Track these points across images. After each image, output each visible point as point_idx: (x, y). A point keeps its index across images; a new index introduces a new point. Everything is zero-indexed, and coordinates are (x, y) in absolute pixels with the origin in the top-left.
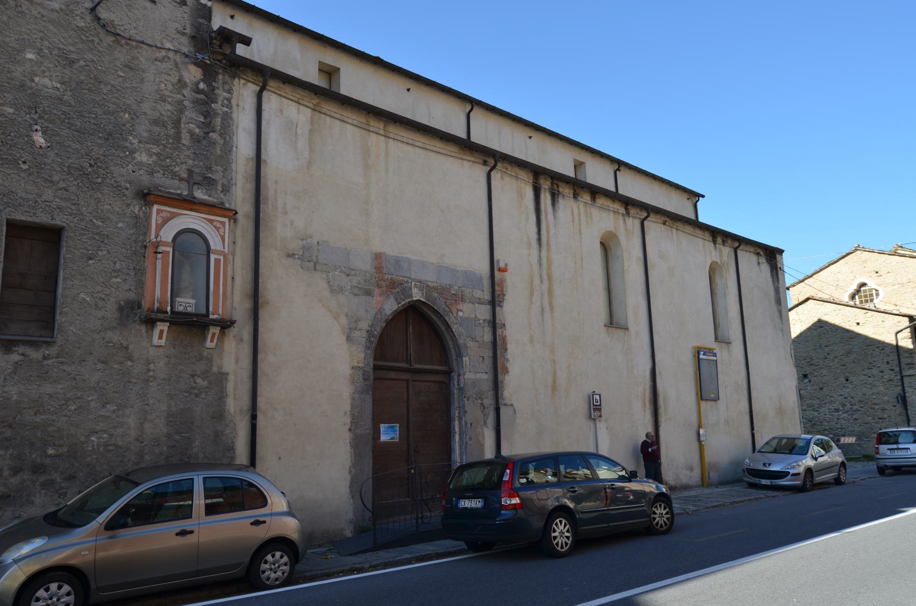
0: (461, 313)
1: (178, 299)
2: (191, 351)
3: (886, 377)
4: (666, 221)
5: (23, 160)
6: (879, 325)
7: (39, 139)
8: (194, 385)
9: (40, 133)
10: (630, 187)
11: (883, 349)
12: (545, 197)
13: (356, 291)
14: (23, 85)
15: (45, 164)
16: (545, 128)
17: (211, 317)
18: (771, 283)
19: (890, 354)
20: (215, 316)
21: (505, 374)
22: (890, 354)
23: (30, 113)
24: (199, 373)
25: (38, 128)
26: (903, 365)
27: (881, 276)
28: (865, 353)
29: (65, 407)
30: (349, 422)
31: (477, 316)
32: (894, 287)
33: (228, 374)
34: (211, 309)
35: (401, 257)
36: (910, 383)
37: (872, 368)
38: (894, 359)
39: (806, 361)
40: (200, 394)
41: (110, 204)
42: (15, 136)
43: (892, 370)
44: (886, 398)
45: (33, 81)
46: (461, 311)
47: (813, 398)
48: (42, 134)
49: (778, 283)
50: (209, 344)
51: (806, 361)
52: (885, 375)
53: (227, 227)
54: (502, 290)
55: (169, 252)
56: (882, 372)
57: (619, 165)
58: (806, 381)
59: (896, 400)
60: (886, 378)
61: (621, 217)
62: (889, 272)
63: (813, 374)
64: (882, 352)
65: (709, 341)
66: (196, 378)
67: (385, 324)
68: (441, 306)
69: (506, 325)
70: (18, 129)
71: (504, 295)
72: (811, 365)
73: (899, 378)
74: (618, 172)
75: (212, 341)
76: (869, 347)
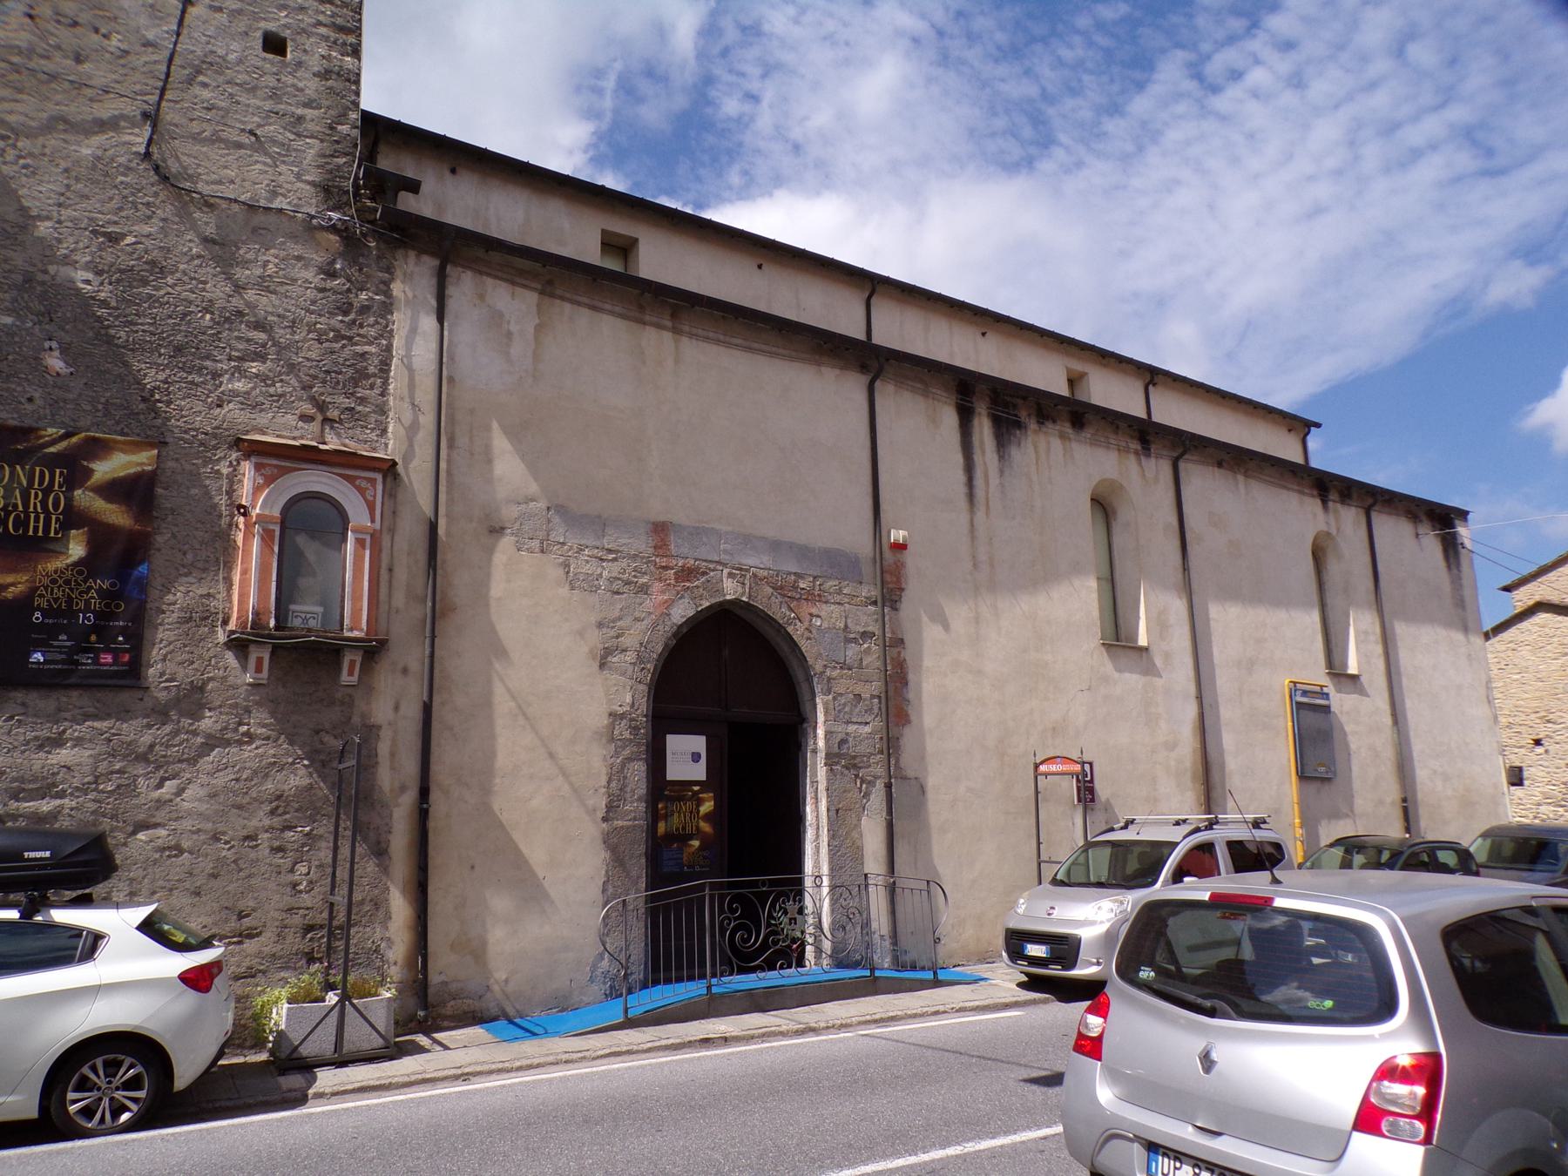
0: (819, 620)
1: (292, 607)
4: (1222, 460)
5: (28, 395)
7: (55, 363)
9: (57, 353)
10: (1172, 412)
12: (981, 424)
13: (615, 587)
14: (29, 279)
15: (65, 401)
16: (888, 278)
17: (347, 634)
18: (1445, 569)
20: (356, 634)
21: (903, 725)
23: (40, 323)
24: (327, 726)
25: (54, 345)
29: (94, 786)
30: (604, 806)
31: (850, 625)
33: (379, 727)
34: (346, 622)
39: (1538, 715)
41: (177, 460)
42: (15, 360)
45: (46, 272)
46: (818, 616)
47: (1554, 782)
48: (61, 354)
49: (1459, 571)
50: (345, 678)
51: (1538, 715)
53: (380, 487)
54: (898, 581)
55: (274, 531)
57: (1152, 376)
58: (1540, 750)
61: (1132, 457)
63: (1551, 738)
65: (1317, 675)
66: (323, 733)
67: (675, 642)
68: (778, 610)
69: (905, 640)
70: (19, 348)
71: (903, 590)
72: (1549, 721)
74: (1151, 387)
75: (351, 673)
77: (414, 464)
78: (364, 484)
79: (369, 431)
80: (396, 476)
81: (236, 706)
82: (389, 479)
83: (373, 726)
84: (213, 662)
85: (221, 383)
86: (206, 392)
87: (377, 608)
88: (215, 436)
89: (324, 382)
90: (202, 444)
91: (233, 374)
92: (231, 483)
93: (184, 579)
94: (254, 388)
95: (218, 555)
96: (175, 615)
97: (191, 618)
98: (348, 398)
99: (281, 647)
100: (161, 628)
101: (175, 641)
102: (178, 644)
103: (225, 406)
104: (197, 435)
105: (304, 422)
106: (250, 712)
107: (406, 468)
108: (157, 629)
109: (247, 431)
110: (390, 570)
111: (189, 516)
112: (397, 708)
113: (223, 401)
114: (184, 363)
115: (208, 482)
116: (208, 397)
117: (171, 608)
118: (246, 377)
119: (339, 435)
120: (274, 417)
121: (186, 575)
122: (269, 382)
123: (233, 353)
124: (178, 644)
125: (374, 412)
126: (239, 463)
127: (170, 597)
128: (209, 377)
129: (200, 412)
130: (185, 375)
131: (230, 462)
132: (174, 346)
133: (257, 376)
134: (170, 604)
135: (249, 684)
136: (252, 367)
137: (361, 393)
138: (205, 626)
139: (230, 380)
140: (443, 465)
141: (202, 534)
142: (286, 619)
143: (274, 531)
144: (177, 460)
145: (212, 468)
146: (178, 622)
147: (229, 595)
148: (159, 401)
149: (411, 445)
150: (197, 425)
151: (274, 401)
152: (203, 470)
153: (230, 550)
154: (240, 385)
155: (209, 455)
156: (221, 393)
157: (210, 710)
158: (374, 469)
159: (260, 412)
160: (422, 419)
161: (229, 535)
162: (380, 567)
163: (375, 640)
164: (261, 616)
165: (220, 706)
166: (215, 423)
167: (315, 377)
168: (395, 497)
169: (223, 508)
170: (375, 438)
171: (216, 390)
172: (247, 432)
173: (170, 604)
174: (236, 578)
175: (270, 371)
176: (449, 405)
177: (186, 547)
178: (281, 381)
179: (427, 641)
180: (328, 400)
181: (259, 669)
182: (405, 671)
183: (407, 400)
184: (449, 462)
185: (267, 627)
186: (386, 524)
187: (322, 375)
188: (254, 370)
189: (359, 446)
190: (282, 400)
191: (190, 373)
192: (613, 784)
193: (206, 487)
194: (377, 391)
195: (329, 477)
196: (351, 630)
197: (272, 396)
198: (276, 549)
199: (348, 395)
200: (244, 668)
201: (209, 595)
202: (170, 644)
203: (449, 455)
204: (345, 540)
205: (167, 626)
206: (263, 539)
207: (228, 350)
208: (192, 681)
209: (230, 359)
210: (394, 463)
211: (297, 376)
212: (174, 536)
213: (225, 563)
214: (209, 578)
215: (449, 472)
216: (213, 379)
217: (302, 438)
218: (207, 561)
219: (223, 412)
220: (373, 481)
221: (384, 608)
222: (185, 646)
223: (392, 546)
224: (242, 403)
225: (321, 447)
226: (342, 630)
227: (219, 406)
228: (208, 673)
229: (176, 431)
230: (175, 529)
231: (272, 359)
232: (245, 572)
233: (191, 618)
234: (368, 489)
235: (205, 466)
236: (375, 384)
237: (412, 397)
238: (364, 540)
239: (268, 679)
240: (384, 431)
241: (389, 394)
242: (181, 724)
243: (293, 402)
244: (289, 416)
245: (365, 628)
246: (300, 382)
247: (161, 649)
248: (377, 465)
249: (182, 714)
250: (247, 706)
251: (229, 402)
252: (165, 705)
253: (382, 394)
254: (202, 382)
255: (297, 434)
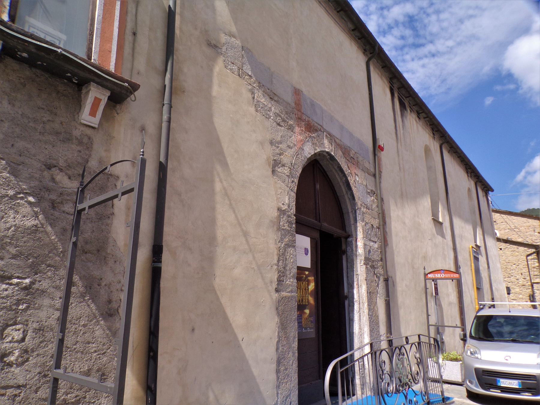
2: (49, 120)
3: (520, 283)
6: (515, 250)
8: (51, 184)
11: (518, 266)
19: (523, 269)
22: (523, 269)
24: (62, 163)
26: (532, 276)
27: (498, 224)
28: (506, 267)
32: (506, 231)
35: (316, 102)
36: (538, 287)
37: (510, 277)
38: (526, 272)
40: (62, 203)
43: (525, 279)
44: (521, 296)
50: (85, 116)
52: (520, 282)
56: (517, 280)
59: (528, 298)
60: (521, 284)
62: (502, 222)
64: (518, 267)
66: (55, 171)
73: (530, 284)
76: (508, 264)
192: (280, 264)
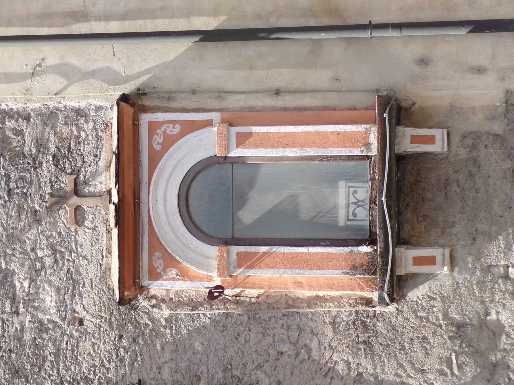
1: (342, 221)
17: (374, 150)
20: (374, 139)
34: (357, 152)
41: (160, 368)
53: (160, 116)
55: (239, 254)
75: (431, 140)
77: (118, 66)
78: (158, 139)
79: (83, 134)
80: (140, 93)
81: (481, 284)
82: (146, 102)
83: (507, 102)
84: (423, 314)
85: (50, 321)
86: (65, 339)
87: (334, 109)
88: (121, 327)
89: (25, 196)
90: (135, 341)
91: (36, 309)
92: (181, 304)
93: (315, 354)
94: (50, 283)
95: (280, 315)
96: (363, 361)
97: (365, 343)
98: (41, 164)
99: (399, 233)
100: (382, 376)
101: (397, 361)
102: (401, 356)
103: (80, 315)
104: (124, 348)
105: (84, 219)
106: (490, 266)
107: (126, 79)
108: (382, 381)
109: (109, 289)
110: (278, 92)
111: (230, 352)
112: (479, 70)
113: (74, 318)
114: (32, 365)
115: (184, 331)
116: (71, 336)
117: (353, 366)
118: (37, 293)
119: (95, 175)
120: (84, 257)
121: (309, 351)
122: (38, 265)
123: (8, 310)
124: (401, 356)
125: (54, 127)
126: (153, 297)
127: (341, 368)
128: (45, 336)
129: (93, 344)
130: (48, 364)
131: (153, 307)
132: (13, 377)
133: (32, 281)
134: (349, 369)
135: (452, 269)
136: (22, 287)
137: (29, 148)
138: (375, 325)
139: (44, 312)
140: (114, 27)
141: (252, 336)
142: (358, 229)
143: (239, 254)
144: (160, 368)
145: (165, 327)
146: (372, 358)
147: (332, 299)
148: (16, 147)
149: (93, 74)
150: (110, 347)
151: (63, 258)
152: (169, 338)
153: (270, 301)
154: (48, 299)
155: (147, 332)
156: (63, 320)
157: (487, 314)
158: (136, 126)
159: (80, 274)
160: (52, 60)
161: (251, 303)
162: (274, 109)
163: (381, 115)
164: (357, 264)
165: (483, 302)
166: (105, 326)
167: (20, 209)
168: (171, 92)
169: (217, 312)
170: (91, 124)
171: (60, 327)
172: (110, 289)
173: (349, 369)
174: (307, 293)
175: (22, 265)
176: (25, 21)
177: (272, 352)
178: (33, 250)
179: (377, 34)
180: (48, 190)
181: (431, 261)
182: (423, 62)
183: (27, 83)
184: (108, 18)
185: (372, 256)
186: (211, 103)
187: (16, 199)
188: (26, 285)
189: (106, 146)
190: (59, 248)
191: (44, 358)
193: (189, 332)
194: (23, 125)
195: (156, 185)
196: (368, 145)
197: (56, 261)
198: (263, 249)
199: (36, 164)
200: (428, 277)
201: (333, 323)
202: (401, 366)
203: (98, 18)
204: (241, 161)
205: (378, 370)
206: (251, 267)
207: (5, 317)
208: (450, 338)
209: (17, 313)
210: (124, 98)
211: (23, 230)
212: (259, 367)
213: (289, 307)
214: (311, 324)
215: (124, 17)
216: (47, 331)
217: (106, 222)
218: (289, 327)
219: (88, 317)
220: (153, 126)
221: (332, 100)
222: (403, 348)
223: (243, 93)
224: (73, 296)
225: (115, 198)
226: (369, 157)
227: (81, 322)
228: (438, 319)
229: (122, 371)
230: (250, 366)
231: (6, 263)
232: (299, 284)
233: (365, 343)
234: (164, 132)
235: (163, 336)
236: (14, 129)
237: (22, 77)
238: (238, 135)
239: (443, 246)
240: (79, 112)
241: (25, 109)
242: (507, 347)
243: (59, 234)
244: (80, 239)
245: (365, 126)
246: (30, 227)
247: (408, 376)
248: (128, 123)
249: (494, 347)
250: (482, 270)
251: (74, 311)
252: (484, 367)
253: (27, 118)
254: (54, 345)
255: (102, 228)
